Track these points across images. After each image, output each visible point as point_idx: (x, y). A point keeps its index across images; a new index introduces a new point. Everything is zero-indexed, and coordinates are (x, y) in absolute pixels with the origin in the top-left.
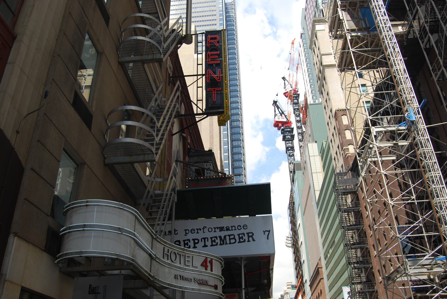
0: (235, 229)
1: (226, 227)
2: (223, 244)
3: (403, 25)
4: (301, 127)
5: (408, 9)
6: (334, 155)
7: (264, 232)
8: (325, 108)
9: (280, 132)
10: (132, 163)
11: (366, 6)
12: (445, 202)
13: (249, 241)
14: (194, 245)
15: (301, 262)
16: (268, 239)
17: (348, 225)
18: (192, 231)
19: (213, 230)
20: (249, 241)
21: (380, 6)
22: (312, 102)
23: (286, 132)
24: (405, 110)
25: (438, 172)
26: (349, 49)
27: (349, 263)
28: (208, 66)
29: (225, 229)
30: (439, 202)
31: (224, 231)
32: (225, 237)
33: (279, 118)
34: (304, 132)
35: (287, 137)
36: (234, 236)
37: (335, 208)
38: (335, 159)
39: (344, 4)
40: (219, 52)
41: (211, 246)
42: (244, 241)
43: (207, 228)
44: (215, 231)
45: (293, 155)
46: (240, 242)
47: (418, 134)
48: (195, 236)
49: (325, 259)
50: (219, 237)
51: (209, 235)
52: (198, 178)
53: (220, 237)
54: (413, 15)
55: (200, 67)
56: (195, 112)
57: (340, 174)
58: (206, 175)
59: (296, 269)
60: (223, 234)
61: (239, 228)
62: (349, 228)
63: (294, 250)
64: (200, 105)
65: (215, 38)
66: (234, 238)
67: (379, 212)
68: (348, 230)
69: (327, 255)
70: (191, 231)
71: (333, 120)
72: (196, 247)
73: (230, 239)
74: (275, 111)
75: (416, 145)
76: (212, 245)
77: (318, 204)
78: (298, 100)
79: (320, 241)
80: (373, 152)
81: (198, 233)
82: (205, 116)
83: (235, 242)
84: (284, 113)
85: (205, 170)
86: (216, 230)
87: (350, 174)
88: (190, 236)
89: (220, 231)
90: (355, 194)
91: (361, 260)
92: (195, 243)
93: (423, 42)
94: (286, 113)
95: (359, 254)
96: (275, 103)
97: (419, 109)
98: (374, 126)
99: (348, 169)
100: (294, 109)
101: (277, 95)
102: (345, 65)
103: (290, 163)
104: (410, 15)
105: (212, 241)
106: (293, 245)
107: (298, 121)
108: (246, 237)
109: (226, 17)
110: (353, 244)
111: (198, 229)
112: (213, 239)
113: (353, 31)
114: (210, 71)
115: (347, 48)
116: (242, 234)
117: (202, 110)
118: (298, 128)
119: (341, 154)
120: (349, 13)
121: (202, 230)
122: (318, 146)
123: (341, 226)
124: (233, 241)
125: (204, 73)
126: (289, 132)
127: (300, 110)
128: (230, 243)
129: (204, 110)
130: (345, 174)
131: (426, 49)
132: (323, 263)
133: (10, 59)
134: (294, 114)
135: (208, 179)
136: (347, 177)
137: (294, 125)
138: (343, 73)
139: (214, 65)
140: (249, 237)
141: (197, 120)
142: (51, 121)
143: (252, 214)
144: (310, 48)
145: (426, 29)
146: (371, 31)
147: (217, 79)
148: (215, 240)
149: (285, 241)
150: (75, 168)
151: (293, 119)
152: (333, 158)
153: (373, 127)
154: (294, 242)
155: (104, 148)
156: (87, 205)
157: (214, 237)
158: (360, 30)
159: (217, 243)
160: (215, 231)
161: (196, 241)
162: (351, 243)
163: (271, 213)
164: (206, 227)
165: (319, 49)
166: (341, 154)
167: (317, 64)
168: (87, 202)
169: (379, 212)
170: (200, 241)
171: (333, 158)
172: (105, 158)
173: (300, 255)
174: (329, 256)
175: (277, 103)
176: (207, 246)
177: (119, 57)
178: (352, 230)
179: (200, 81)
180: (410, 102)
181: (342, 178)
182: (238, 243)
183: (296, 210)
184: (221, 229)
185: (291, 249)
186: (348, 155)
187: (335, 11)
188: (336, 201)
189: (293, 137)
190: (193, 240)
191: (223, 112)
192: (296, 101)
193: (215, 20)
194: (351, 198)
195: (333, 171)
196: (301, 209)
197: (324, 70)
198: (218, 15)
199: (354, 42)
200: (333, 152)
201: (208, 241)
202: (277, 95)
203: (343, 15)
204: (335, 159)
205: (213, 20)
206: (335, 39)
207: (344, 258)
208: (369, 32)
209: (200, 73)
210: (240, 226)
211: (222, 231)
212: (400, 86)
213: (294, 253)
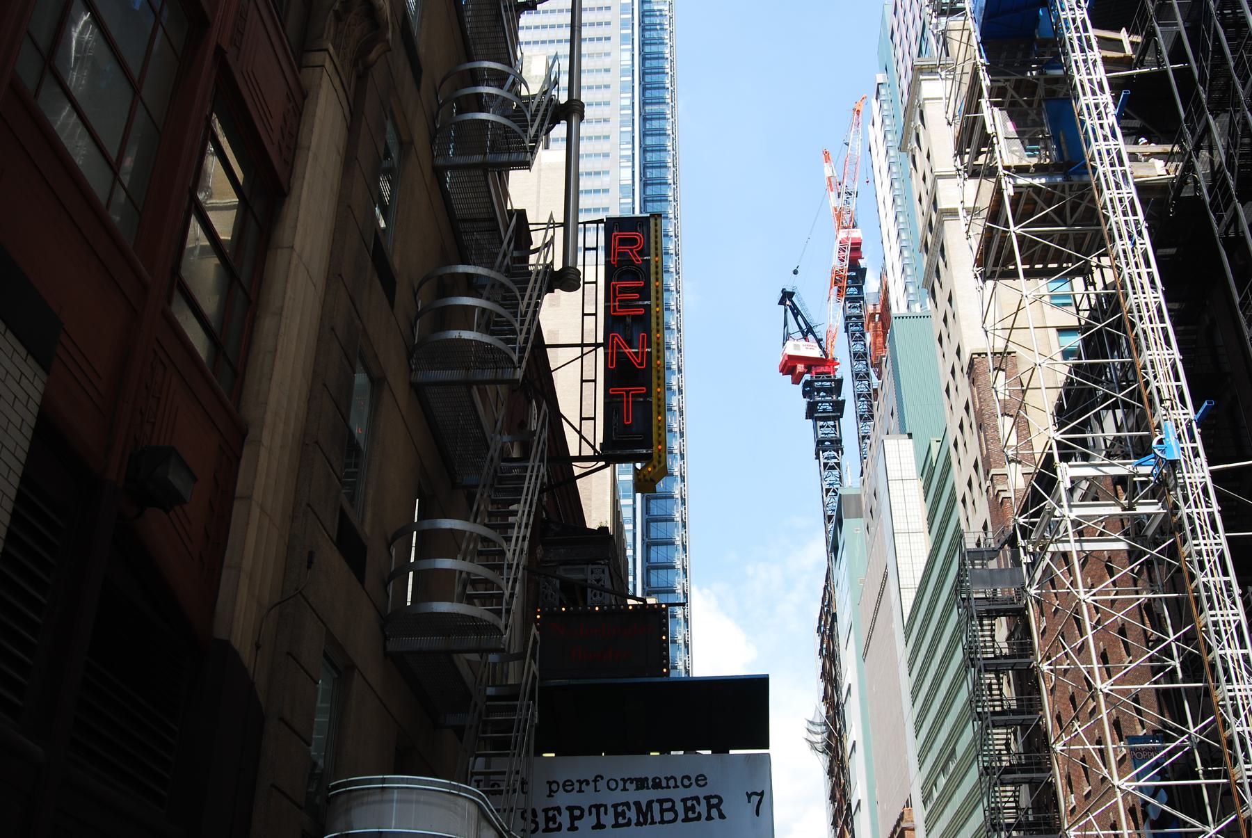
0: (676, 786)
1: (654, 780)
2: (645, 823)
3: (1167, 157)
4: (868, 374)
5: (1183, 115)
6: (961, 489)
7: (749, 796)
8: (940, 340)
9: (799, 388)
11: (1061, 96)
12: (1247, 697)
13: (709, 818)
15: (849, 806)
17: (998, 709)
18: (567, 786)
19: (621, 784)
20: (709, 818)
21: (1102, 108)
22: (903, 310)
23: (819, 390)
24: (1156, 423)
25: (1235, 611)
26: (1007, 225)
27: (993, 826)
28: (612, 322)
29: (650, 783)
30: (1232, 698)
32: (650, 803)
33: (797, 347)
34: (875, 391)
35: (821, 407)
36: (673, 803)
37: (959, 655)
38: (964, 501)
39: (1001, 84)
40: (641, 283)
41: (613, 826)
42: (698, 818)
44: (625, 789)
45: (838, 464)
46: (686, 819)
47: (1186, 499)
49: (925, 803)
50: (635, 803)
53: (637, 804)
54: (1196, 138)
55: (589, 321)
56: (574, 452)
57: (979, 553)
59: (835, 824)
60: (644, 796)
61: (686, 782)
62: (1000, 718)
63: (831, 762)
64: (587, 427)
65: (633, 241)
66: (672, 809)
67: (1072, 699)
68: (995, 727)
69: (931, 792)
70: (564, 785)
71: (963, 381)
72: (576, 829)
73: (662, 811)
74: (786, 324)
75: (1180, 527)
76: (616, 825)
77: (908, 631)
78: (860, 289)
79: (912, 746)
80: (1062, 529)
81: (580, 791)
82: (602, 463)
83: (674, 820)
84: (815, 330)
87: (1009, 554)
88: (563, 799)
89: (637, 789)
90: (1018, 616)
91: (1031, 818)
92: (573, 818)
93: (1219, 219)
94: (821, 332)
95: (1025, 800)
96: (787, 296)
97: (1194, 424)
98: (1067, 461)
99: (1003, 538)
100: (847, 318)
101: (795, 272)
102: (994, 262)
103: (828, 491)
104: (1189, 137)
105: (617, 815)
106: (828, 746)
107: (857, 356)
108: (702, 808)
109: (643, 15)
110: (1007, 770)
111: (580, 782)
113: (1022, 170)
114: (618, 338)
115: (1002, 221)
116: (692, 798)
117: (593, 447)
118: (858, 376)
119: (984, 488)
120: (1012, 117)
121: (592, 784)
122: (915, 447)
123: (974, 711)
124: (669, 816)
125: (600, 340)
126: (829, 391)
127: (866, 320)
128: (662, 822)
129: (598, 448)
130: (994, 553)
131: (1227, 243)
132: (919, 814)
133: (240, 489)
134: (847, 331)
136: (999, 562)
137: (844, 370)
138: (990, 283)
139: (629, 320)
140: (710, 807)
142: (306, 600)
144: (902, 148)
145: (1228, 185)
146: (1074, 173)
147: (635, 361)
149: (805, 734)
151: (841, 350)
152: (959, 499)
153: (1064, 465)
154: (829, 737)
157: (623, 804)
158: (1040, 170)
160: (625, 789)
161: (577, 813)
162: (1004, 764)
163: (767, 747)
165: (928, 157)
166: (984, 488)
167: (920, 200)
168: (383, 781)
169: (1072, 699)
170: (586, 812)
171: (959, 499)
172: (386, 639)
173: (848, 782)
174: (936, 794)
175: (794, 299)
176: (604, 826)
177: (411, 370)
178: (1006, 726)
179: (589, 359)
180: (1168, 403)
181: (982, 565)
183: (842, 640)
184: (641, 783)
185: (824, 756)
186: (1003, 495)
187: (973, 103)
188: (962, 632)
189: (839, 407)
192: (853, 291)
193: (608, 23)
194: (1009, 629)
195: (959, 536)
196: (856, 641)
197: (941, 223)
198: (616, 24)
199: (1025, 204)
200: (959, 477)
201: (606, 813)
202: (795, 272)
203: (997, 121)
204: (964, 501)
205: (600, 24)
206: (970, 177)
207: (980, 808)
208: (1067, 178)
209: (589, 339)
210: (689, 778)
211: (642, 788)
212: (1146, 353)
213: (830, 772)
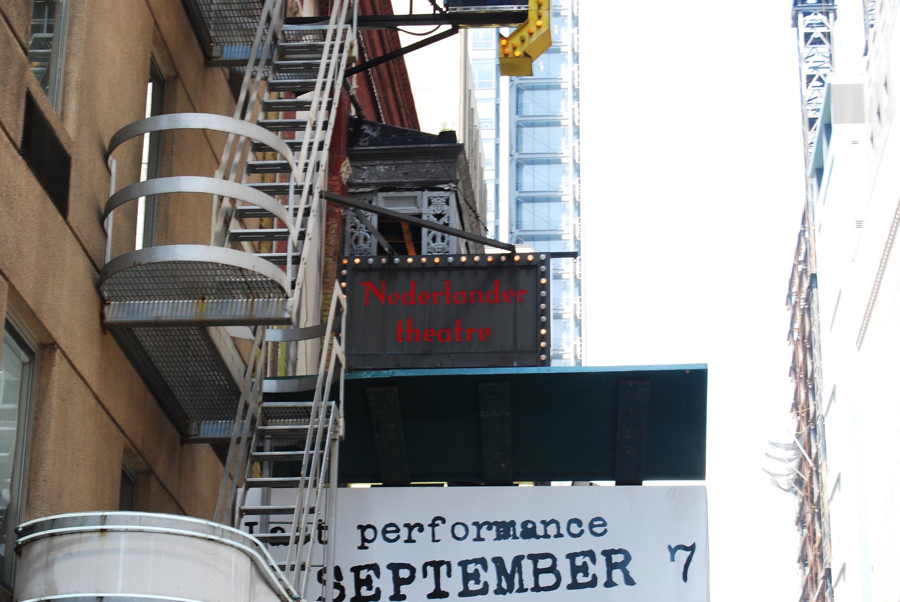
0: (559, 535)
1: (524, 524)
2: (510, 589)
7: (673, 551)
10: (203, 326)
13: (610, 583)
14: (397, 589)
15: (828, 572)
16: (685, 578)
18: (390, 531)
19: (473, 530)
20: (610, 583)
29: (519, 530)
31: (515, 537)
32: (518, 561)
36: (554, 559)
41: (461, 594)
42: (593, 583)
43: (449, 524)
44: (479, 539)
48: (399, 552)
51: (453, 551)
52: (391, 260)
53: (499, 561)
58: (424, 251)
60: (509, 549)
61: (575, 529)
63: (802, 505)
66: (552, 569)
70: (385, 532)
73: (537, 572)
76: (465, 593)
81: (410, 540)
82: (447, 27)
83: (556, 586)
85: (425, 231)
86: (484, 531)
89: (499, 538)
103: (810, 78)
105: (466, 577)
106: (799, 482)
108: (599, 569)
111: (410, 527)
112: (471, 569)
116: (584, 554)
121: (428, 530)
124: (547, 580)
128: (537, 588)
135: (436, 268)
140: (611, 567)
141: (403, 45)
143: (629, 477)
148: (476, 573)
150: (24, 364)
154: (800, 468)
155: (106, 277)
156: (103, 531)
157: (475, 561)
159: (486, 585)
161: (404, 573)
164: (444, 521)
170: (419, 573)
172: (103, 302)
176: (445, 595)
182: (570, 587)
184: (504, 530)
190: (391, 566)
191: (521, 18)
201: (449, 574)
210: (579, 523)
211: (506, 537)
